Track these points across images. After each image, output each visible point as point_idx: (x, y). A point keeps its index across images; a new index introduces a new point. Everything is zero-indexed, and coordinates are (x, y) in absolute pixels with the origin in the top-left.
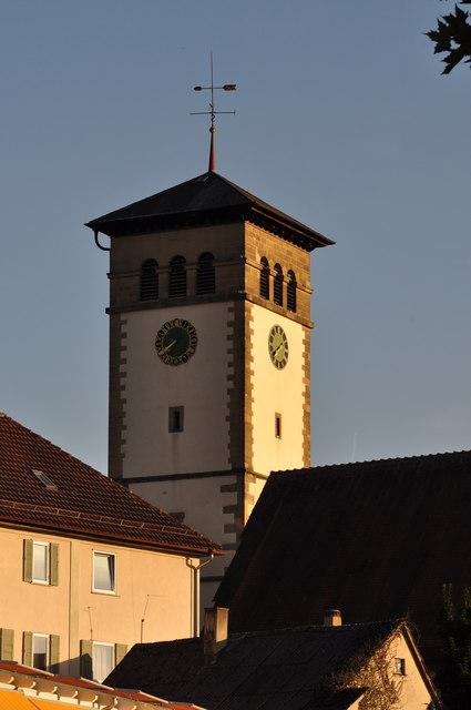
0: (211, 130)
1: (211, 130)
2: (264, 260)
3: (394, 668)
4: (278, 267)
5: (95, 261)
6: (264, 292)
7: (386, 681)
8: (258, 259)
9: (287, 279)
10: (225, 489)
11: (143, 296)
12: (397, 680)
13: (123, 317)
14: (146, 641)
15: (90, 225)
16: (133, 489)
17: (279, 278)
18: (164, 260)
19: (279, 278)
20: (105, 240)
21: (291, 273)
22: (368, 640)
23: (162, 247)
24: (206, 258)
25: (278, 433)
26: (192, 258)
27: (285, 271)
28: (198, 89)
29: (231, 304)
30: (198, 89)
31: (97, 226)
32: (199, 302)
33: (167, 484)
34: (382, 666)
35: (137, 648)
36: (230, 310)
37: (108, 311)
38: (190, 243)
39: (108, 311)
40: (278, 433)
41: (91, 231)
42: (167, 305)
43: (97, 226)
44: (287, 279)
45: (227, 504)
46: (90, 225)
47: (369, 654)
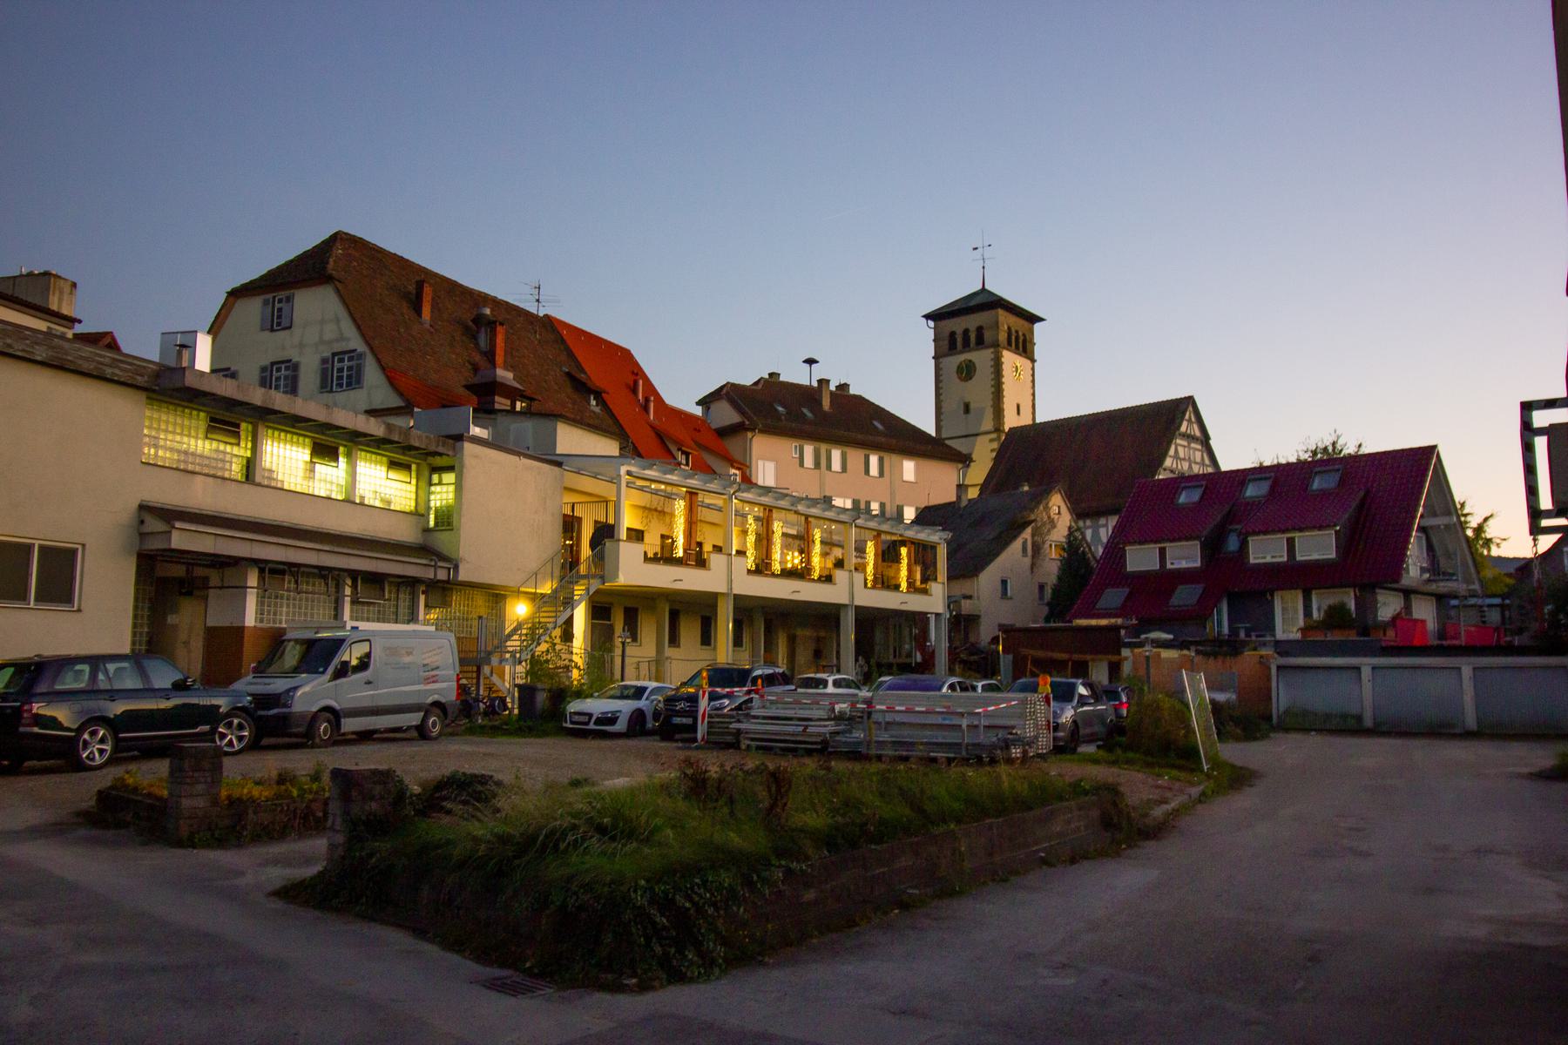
0: (984, 267)
1: (984, 267)
2: (1009, 328)
3: (1055, 509)
4: (1017, 332)
5: (927, 332)
6: (1009, 343)
7: (1049, 517)
8: (1006, 328)
9: (1021, 338)
10: (992, 440)
11: (950, 349)
12: (1056, 517)
13: (941, 360)
14: (931, 504)
15: (924, 316)
16: (947, 442)
17: (1017, 338)
18: (959, 331)
19: (1017, 338)
20: (931, 324)
21: (1024, 335)
22: (1040, 497)
23: (957, 325)
24: (980, 330)
25: (1018, 413)
26: (973, 329)
27: (1020, 334)
28: (990, 245)
29: (992, 350)
30: (990, 245)
31: (928, 317)
32: (977, 350)
33: (963, 440)
34: (1047, 508)
35: (926, 507)
36: (992, 353)
37: (933, 358)
38: (971, 322)
39: (933, 358)
40: (1018, 413)
41: (924, 320)
42: (961, 352)
43: (928, 317)
44: (1021, 338)
45: (992, 448)
46: (924, 316)
47: (1039, 503)
